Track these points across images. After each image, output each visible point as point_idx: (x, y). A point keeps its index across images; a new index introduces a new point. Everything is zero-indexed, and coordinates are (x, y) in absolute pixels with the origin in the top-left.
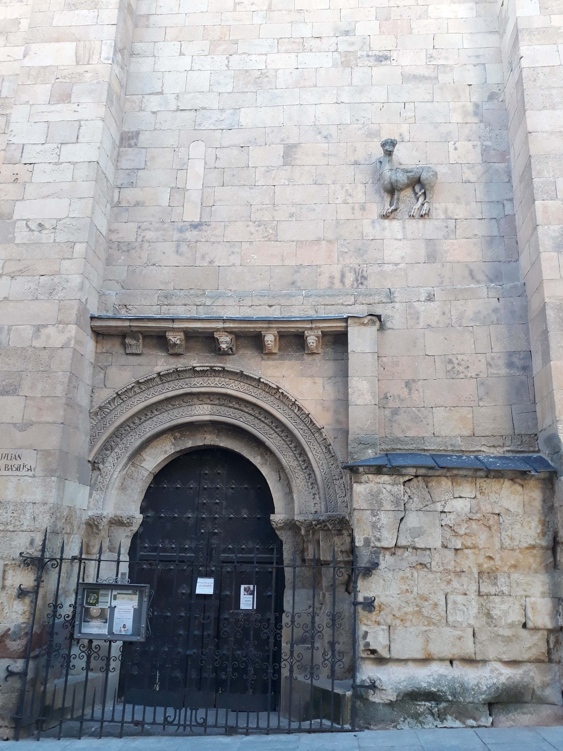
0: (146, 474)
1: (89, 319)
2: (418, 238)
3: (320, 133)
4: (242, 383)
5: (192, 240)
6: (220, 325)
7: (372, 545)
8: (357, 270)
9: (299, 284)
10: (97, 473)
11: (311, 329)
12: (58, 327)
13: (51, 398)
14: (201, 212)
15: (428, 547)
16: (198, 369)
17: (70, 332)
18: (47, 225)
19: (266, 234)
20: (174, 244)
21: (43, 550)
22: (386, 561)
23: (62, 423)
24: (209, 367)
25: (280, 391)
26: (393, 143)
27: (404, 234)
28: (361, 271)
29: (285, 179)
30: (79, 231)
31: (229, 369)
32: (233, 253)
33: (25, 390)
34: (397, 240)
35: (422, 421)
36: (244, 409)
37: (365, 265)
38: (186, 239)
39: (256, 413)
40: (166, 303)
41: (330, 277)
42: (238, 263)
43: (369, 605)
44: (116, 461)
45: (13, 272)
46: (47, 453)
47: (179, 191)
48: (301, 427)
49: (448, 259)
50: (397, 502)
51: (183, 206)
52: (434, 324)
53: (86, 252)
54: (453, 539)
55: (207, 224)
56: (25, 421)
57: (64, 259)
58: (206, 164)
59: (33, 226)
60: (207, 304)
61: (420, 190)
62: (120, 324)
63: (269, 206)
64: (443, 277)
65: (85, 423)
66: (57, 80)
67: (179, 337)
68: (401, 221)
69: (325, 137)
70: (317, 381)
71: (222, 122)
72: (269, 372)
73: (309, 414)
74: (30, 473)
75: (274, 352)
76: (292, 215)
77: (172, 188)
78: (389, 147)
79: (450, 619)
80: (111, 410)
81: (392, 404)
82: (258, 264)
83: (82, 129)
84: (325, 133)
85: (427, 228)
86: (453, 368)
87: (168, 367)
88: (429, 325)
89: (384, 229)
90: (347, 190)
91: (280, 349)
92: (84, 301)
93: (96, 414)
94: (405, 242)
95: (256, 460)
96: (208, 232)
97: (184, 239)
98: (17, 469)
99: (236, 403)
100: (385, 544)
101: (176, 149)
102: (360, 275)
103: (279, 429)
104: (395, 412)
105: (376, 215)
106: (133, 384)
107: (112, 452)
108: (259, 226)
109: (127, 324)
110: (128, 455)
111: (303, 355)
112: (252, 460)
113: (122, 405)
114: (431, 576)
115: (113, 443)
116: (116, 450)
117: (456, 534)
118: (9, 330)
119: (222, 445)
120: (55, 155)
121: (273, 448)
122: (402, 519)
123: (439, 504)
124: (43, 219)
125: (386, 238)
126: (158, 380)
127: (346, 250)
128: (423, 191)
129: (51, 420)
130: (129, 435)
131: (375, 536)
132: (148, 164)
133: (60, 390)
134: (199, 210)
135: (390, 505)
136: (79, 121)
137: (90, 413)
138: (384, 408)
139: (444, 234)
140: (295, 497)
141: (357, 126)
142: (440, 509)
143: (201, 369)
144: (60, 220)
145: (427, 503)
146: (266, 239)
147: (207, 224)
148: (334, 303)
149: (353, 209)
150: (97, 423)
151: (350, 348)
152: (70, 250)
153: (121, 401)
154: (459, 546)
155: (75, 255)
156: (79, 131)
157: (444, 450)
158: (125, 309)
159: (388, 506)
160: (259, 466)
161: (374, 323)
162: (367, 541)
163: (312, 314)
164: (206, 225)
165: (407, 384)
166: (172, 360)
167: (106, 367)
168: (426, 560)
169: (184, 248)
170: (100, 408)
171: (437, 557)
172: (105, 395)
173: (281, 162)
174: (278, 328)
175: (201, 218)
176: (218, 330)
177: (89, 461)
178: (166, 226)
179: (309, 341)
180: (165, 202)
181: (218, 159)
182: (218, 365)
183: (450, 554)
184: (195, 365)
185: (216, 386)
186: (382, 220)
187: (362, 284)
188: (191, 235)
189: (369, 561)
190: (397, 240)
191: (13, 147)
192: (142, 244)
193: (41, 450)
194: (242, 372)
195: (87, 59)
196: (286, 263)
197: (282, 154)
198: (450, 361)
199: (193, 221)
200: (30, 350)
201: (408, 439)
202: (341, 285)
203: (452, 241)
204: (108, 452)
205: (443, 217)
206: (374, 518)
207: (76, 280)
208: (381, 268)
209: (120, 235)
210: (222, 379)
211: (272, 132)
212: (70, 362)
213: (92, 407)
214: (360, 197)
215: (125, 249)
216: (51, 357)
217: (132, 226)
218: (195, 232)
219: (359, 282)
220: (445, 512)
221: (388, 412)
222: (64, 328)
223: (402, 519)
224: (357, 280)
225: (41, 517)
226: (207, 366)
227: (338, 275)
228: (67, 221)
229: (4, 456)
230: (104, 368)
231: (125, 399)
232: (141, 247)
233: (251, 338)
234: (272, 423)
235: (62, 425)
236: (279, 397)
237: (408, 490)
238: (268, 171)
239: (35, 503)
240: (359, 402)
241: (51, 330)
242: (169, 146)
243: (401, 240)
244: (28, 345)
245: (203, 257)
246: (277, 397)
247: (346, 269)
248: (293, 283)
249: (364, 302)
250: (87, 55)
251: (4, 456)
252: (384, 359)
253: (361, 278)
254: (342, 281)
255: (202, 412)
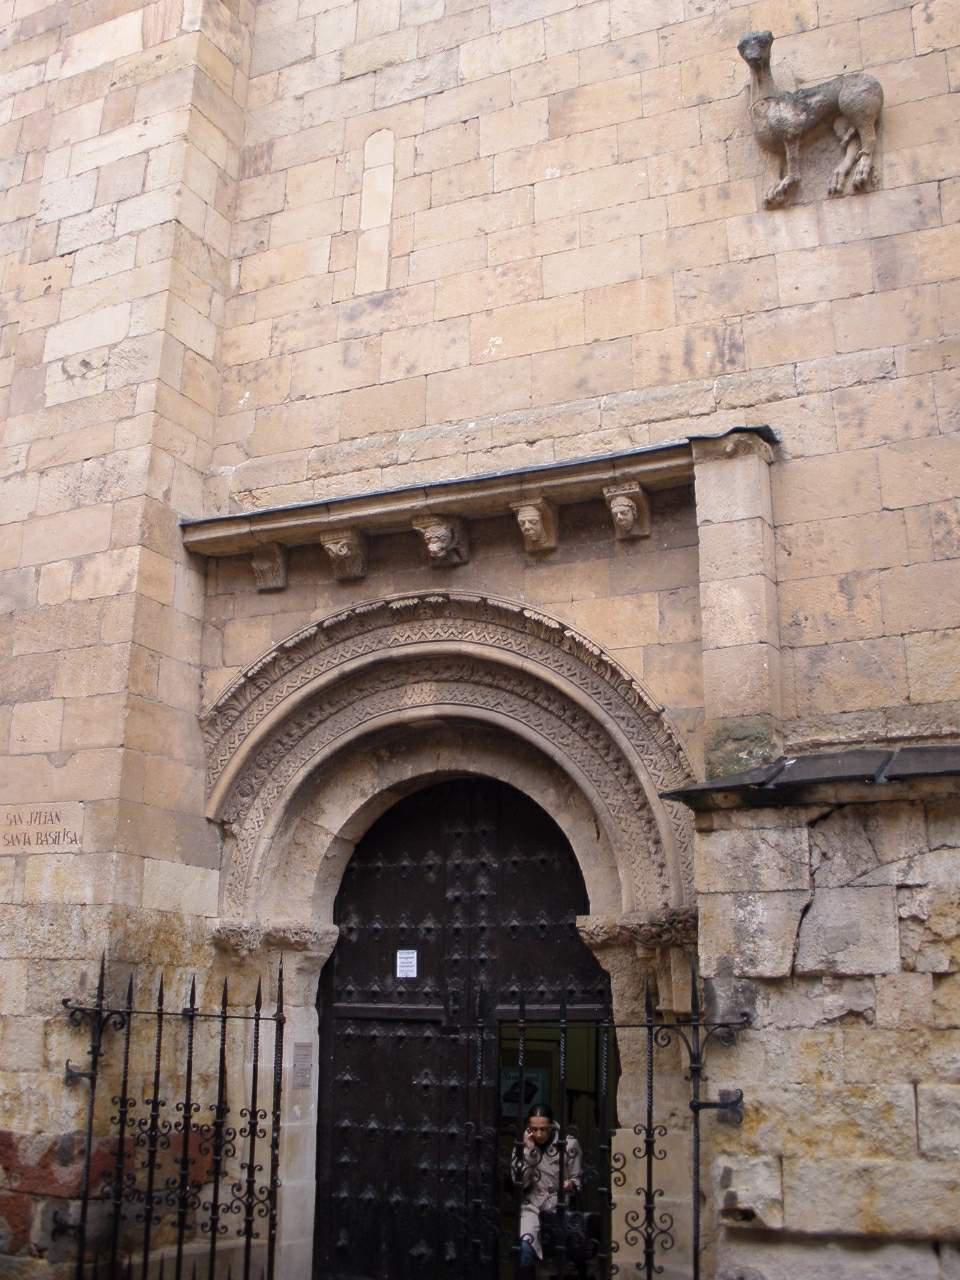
0: (327, 841)
1: (179, 531)
2: (853, 238)
3: (621, 56)
4: (490, 626)
5: (372, 332)
6: (419, 503)
7: (737, 972)
8: (720, 331)
9: (591, 385)
10: (231, 843)
11: (614, 482)
12: (111, 556)
13: (103, 698)
14: (389, 271)
15: (868, 971)
16: (395, 605)
17: (130, 561)
18: (95, 363)
19: (518, 290)
20: (339, 346)
21: (101, 995)
22: (765, 1011)
23: (122, 746)
24: (419, 597)
25: (568, 633)
26: (765, 42)
27: (822, 237)
28: (728, 332)
29: (552, 166)
30: (145, 360)
31: (458, 598)
32: (454, 341)
33: (63, 688)
34: (805, 250)
35: (880, 670)
36: (503, 684)
37: (738, 319)
38: (362, 331)
39: (528, 690)
40: (323, 473)
41: (662, 357)
42: (464, 362)
43: (732, 1109)
44: (262, 817)
45: (43, 463)
46: (95, 806)
47: (346, 236)
48: (622, 714)
49: (927, 276)
50: (791, 867)
51: (355, 267)
52: (897, 432)
53: (157, 398)
54: (929, 951)
55: (401, 293)
56: (64, 747)
57: (121, 419)
58: (396, 172)
59: (74, 367)
60: (402, 459)
61: (847, 130)
62: (232, 531)
63: (524, 228)
64: (919, 319)
65: (181, 739)
66: (113, 88)
67: (344, 541)
68: (811, 208)
69: (634, 61)
70: (646, 602)
71: (426, 82)
72: (542, 594)
73: (632, 680)
74: (75, 848)
75: (546, 545)
76: (571, 239)
77: (334, 236)
78: (758, 55)
79: (924, 1146)
80: (242, 713)
81: (810, 636)
82: (505, 355)
83: (152, 163)
84: (631, 53)
85: (879, 213)
86: (949, 533)
87: (337, 609)
88: (886, 438)
89: (774, 232)
90: (686, 164)
91: (561, 539)
92: (159, 495)
93: (212, 722)
94: (824, 251)
95: (545, 797)
96: (404, 308)
97: (357, 333)
98: (54, 841)
99: (487, 674)
100: (767, 969)
101: (340, 158)
102: (727, 342)
103: (581, 723)
104: (818, 655)
105: (753, 202)
106: (274, 654)
107: (254, 799)
108: (504, 274)
109: (245, 529)
110: (283, 802)
111: (613, 543)
112: (537, 798)
113: (261, 698)
114: (874, 1040)
115: (254, 781)
116: (262, 795)
117: (937, 939)
118: (38, 573)
119: (472, 769)
120: (109, 227)
121: (571, 767)
122: (806, 910)
123: (895, 867)
124: (89, 353)
125: (779, 250)
126: (322, 638)
127: (693, 292)
128: (852, 131)
129: (103, 741)
130: (285, 760)
131: (742, 953)
132: (289, 199)
133: (116, 680)
134: (386, 268)
135: (777, 878)
136: (146, 152)
137: (200, 721)
138: (791, 648)
139: (912, 218)
140: (621, 875)
141: (699, 22)
142: (895, 876)
143: (402, 603)
144: (115, 345)
145: (864, 868)
146: (521, 298)
147: (401, 293)
148: (668, 415)
149: (702, 200)
150: (218, 741)
151: (701, 513)
152: (131, 400)
153: (258, 692)
154: (944, 967)
155: (139, 409)
156: (145, 171)
157: (934, 736)
158: (250, 499)
159: (770, 878)
160: (551, 811)
161: (748, 449)
162: (725, 968)
163: (624, 447)
164: (399, 294)
165: (844, 585)
166: (345, 593)
167: (224, 623)
168: (864, 1003)
169: (357, 351)
170: (217, 709)
171: (889, 993)
172: (223, 681)
173: (543, 133)
174: (542, 489)
175: (388, 284)
176: (417, 514)
177: (209, 820)
178: (323, 313)
179: (614, 510)
180: (322, 266)
181: (419, 158)
182: (435, 591)
183: (920, 986)
184: (389, 597)
185: (437, 638)
186: (769, 213)
187: (732, 361)
188: (370, 321)
189: (731, 1012)
190: (805, 250)
191: (45, 229)
192: (280, 360)
193: (90, 802)
194: (484, 600)
195: (159, 34)
196: (564, 342)
197: (545, 116)
198: (941, 518)
199: (373, 293)
200: (69, 606)
201: (852, 716)
202: (686, 371)
203: (934, 231)
204: (245, 799)
205: (906, 179)
206: (741, 911)
207: (140, 458)
208: (773, 320)
209: (242, 351)
210: (450, 622)
211: (524, 76)
212: (131, 621)
213: (202, 708)
214: (717, 172)
215: (250, 376)
216: (101, 616)
217: (263, 327)
218: (379, 313)
219: (727, 358)
220: (907, 887)
221: (801, 658)
222: (120, 557)
223: (806, 910)
224: (721, 355)
225: (94, 931)
226: (413, 598)
227: (678, 351)
228: (126, 346)
229: (34, 816)
230: (220, 627)
231: (265, 686)
232: (279, 367)
233: (482, 521)
234: (565, 710)
235: (121, 750)
236: (570, 648)
237: (820, 840)
238: (518, 158)
239: (84, 905)
240: (724, 641)
241: (101, 564)
242: (328, 154)
243: (813, 249)
244: (66, 598)
245: (395, 362)
246: (566, 648)
247: (696, 335)
248: (582, 384)
249: (736, 402)
250: (160, 27)
251: (34, 816)
252: (789, 531)
253: (730, 350)
254: (688, 363)
255: (420, 702)
